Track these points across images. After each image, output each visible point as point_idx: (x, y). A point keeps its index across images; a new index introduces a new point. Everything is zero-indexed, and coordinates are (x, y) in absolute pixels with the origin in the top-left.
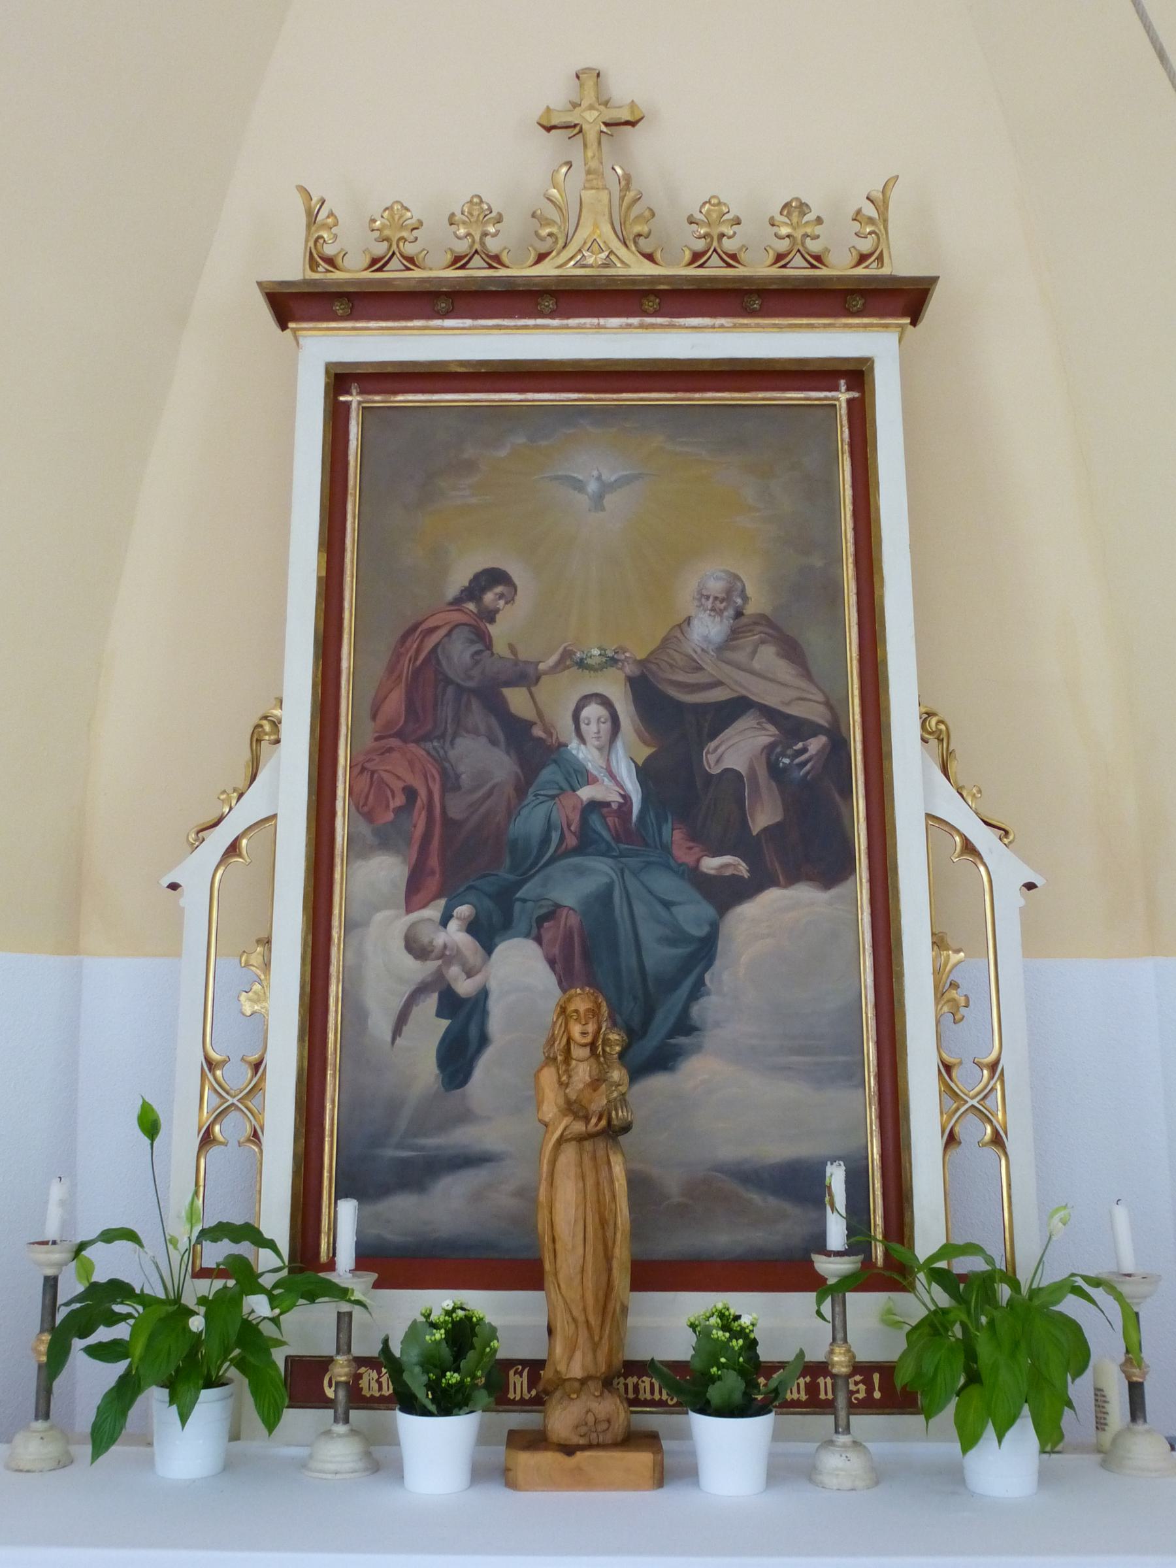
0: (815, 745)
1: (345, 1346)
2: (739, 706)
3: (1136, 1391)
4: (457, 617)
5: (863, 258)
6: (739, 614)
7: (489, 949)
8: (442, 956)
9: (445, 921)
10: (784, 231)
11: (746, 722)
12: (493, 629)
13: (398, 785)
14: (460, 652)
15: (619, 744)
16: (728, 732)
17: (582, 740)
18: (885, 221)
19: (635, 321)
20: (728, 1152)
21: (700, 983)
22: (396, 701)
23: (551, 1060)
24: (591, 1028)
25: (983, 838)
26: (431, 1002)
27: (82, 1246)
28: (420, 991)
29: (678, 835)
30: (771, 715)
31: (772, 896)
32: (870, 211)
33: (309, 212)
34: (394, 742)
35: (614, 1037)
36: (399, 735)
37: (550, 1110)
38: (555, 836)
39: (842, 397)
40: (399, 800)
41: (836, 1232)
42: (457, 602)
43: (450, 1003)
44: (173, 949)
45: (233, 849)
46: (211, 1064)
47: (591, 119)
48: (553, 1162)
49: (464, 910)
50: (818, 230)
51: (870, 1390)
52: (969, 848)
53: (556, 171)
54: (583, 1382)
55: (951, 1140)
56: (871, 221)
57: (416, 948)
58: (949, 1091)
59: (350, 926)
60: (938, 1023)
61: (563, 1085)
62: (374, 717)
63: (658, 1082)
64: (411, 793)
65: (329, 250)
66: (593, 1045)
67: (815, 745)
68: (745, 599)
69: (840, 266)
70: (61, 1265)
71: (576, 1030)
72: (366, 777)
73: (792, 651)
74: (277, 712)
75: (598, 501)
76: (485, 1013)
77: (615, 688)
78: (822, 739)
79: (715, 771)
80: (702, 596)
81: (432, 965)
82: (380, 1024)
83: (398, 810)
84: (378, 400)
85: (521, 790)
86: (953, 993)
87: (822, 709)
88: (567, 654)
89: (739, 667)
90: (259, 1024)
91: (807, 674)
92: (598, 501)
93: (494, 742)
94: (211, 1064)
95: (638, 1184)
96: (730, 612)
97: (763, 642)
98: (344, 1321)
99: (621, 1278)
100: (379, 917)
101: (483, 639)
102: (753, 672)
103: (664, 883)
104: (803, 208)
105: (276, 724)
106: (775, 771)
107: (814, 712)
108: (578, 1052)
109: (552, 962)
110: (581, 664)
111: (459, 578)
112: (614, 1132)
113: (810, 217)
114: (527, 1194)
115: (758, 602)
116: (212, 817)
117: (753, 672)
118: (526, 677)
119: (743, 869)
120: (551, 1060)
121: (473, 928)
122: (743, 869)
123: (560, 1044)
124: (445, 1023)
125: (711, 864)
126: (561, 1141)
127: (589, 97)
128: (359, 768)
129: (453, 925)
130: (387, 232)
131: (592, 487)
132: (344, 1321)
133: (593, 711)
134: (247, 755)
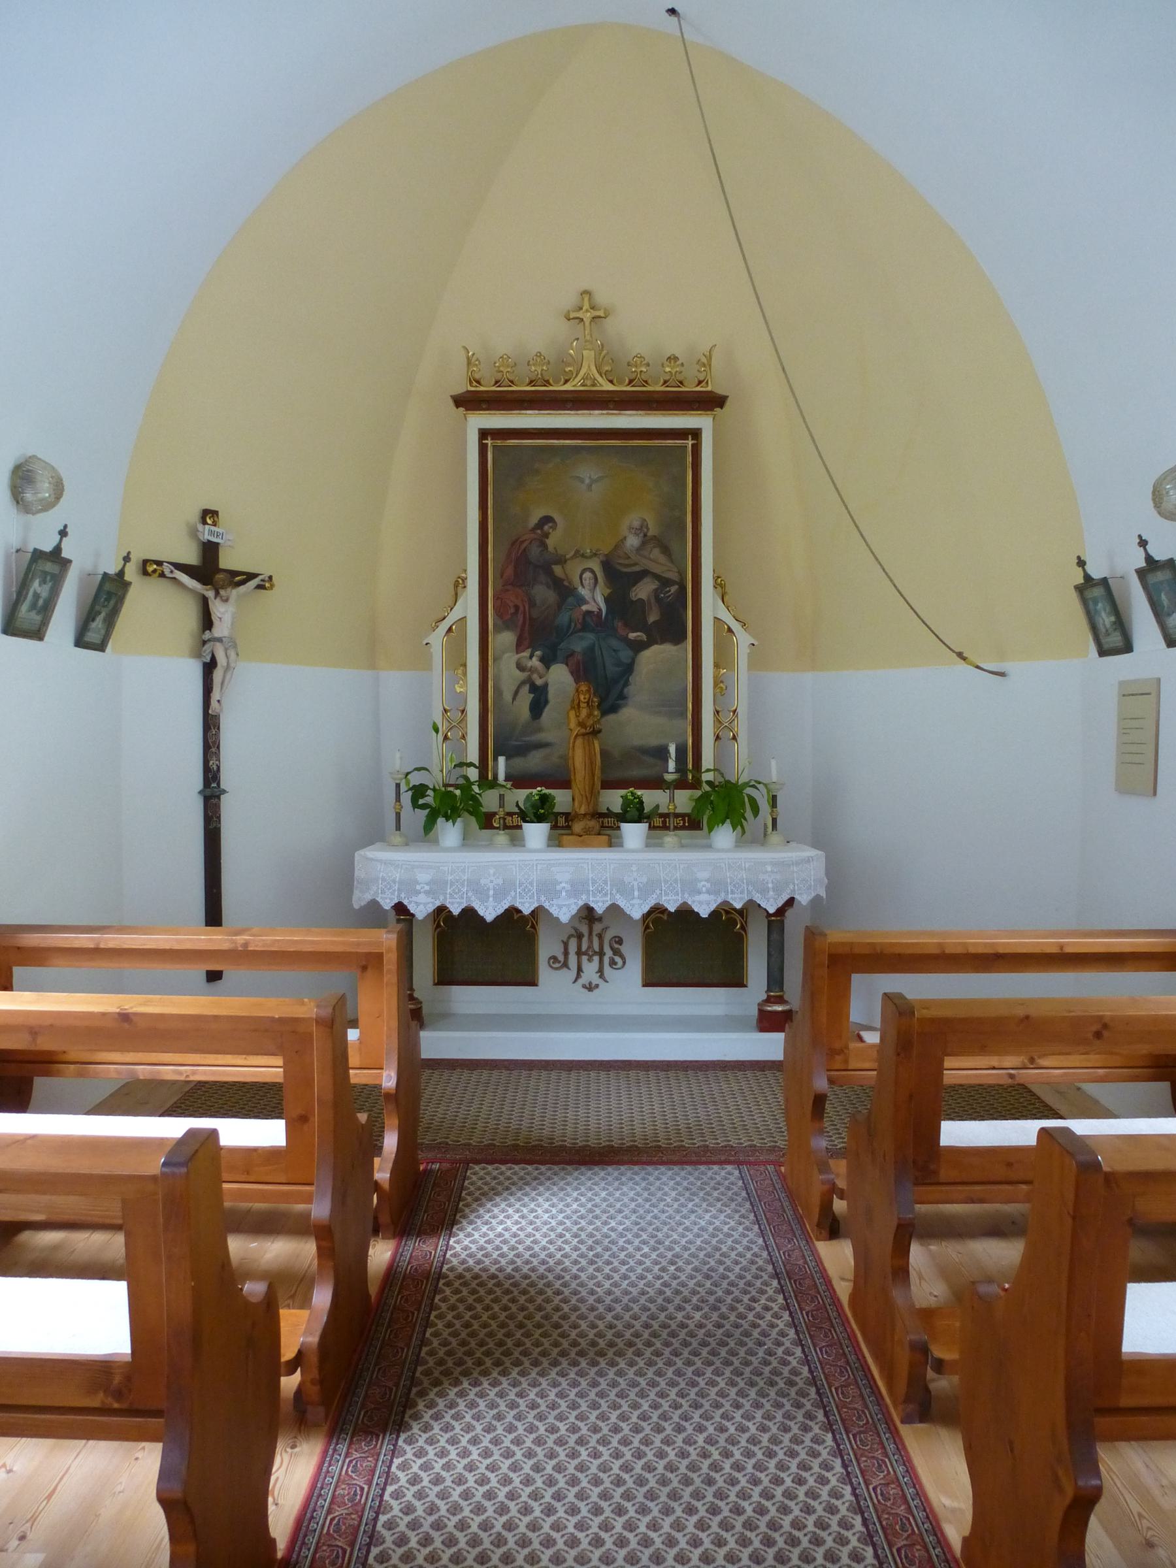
0: (674, 589)
1: (502, 805)
2: (645, 573)
3: (774, 821)
4: (532, 535)
5: (700, 382)
6: (645, 535)
7: (548, 668)
8: (530, 670)
9: (531, 657)
10: (668, 369)
11: (647, 580)
12: (548, 541)
13: (511, 604)
14: (535, 551)
15: (598, 588)
16: (641, 583)
17: (583, 586)
18: (710, 365)
19: (605, 412)
20: (637, 742)
21: (627, 680)
22: (510, 571)
23: (573, 708)
24: (587, 696)
25: (735, 626)
26: (527, 688)
27: (408, 774)
28: (523, 683)
29: (620, 624)
30: (657, 577)
31: (655, 648)
32: (704, 360)
33: (468, 358)
34: (509, 587)
35: (595, 700)
36: (511, 584)
37: (573, 725)
38: (573, 624)
39: (690, 442)
40: (512, 610)
41: (672, 765)
42: (533, 530)
43: (534, 688)
44: (428, 667)
45: (450, 629)
46: (446, 711)
47: (587, 317)
48: (574, 742)
49: (538, 653)
50: (682, 369)
51: (684, 823)
52: (730, 630)
53: (572, 343)
54: (585, 815)
55: (718, 738)
56: (704, 365)
57: (520, 667)
58: (718, 722)
59: (495, 660)
60: (714, 696)
61: (577, 716)
62: (502, 577)
63: (611, 717)
64: (517, 608)
65: (477, 376)
66: (588, 703)
67: (674, 589)
68: (648, 529)
69: (690, 387)
70: (401, 779)
71: (582, 697)
72: (499, 601)
73: (666, 550)
74: (464, 575)
75: (589, 487)
76: (547, 693)
77: (596, 565)
78: (676, 587)
79: (634, 599)
80: (630, 528)
81: (526, 674)
82: (508, 696)
83: (513, 614)
84: (499, 443)
85: (560, 606)
86: (721, 685)
87: (677, 574)
88: (577, 552)
89: (645, 557)
90: (464, 697)
91: (672, 561)
92: (589, 487)
93: (549, 587)
94: (446, 711)
95: (604, 754)
96: (642, 535)
97: (654, 547)
98: (502, 797)
99: (598, 784)
100: (506, 655)
101: (544, 545)
102: (650, 560)
103: (614, 643)
104: (676, 359)
105: (464, 580)
106: (658, 599)
107: (673, 576)
108: (582, 705)
109: (572, 673)
110: (583, 556)
111: (534, 520)
112: (595, 733)
113: (679, 362)
114: (565, 758)
115: (653, 531)
116: (441, 616)
117: (650, 560)
118: (562, 561)
119: (644, 637)
120: (573, 708)
121: (542, 660)
122: (644, 637)
123: (576, 702)
124: (532, 696)
125: (632, 636)
126: (577, 735)
127: (586, 306)
128: (496, 598)
129: (534, 659)
130: (501, 369)
131: (587, 481)
132: (502, 797)
133: (587, 575)
134: (453, 593)
